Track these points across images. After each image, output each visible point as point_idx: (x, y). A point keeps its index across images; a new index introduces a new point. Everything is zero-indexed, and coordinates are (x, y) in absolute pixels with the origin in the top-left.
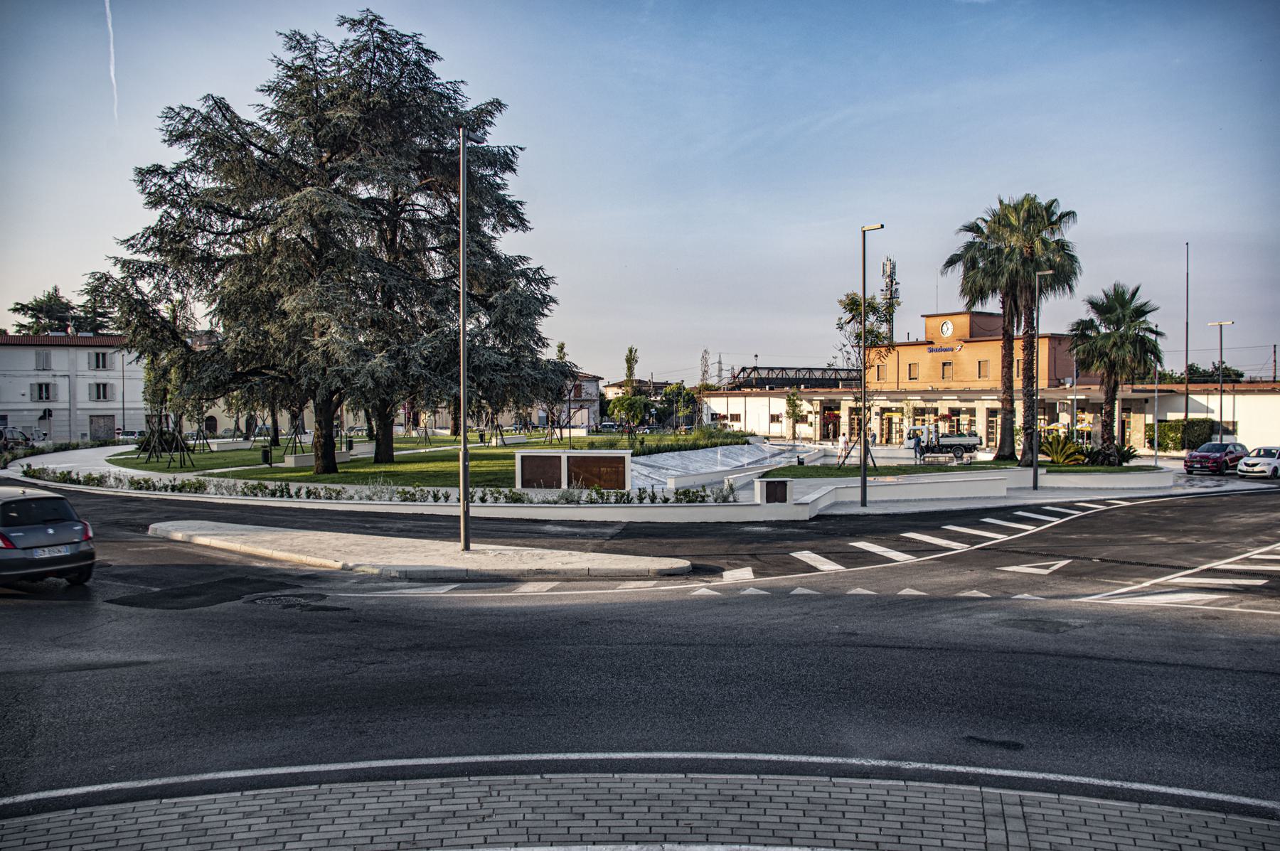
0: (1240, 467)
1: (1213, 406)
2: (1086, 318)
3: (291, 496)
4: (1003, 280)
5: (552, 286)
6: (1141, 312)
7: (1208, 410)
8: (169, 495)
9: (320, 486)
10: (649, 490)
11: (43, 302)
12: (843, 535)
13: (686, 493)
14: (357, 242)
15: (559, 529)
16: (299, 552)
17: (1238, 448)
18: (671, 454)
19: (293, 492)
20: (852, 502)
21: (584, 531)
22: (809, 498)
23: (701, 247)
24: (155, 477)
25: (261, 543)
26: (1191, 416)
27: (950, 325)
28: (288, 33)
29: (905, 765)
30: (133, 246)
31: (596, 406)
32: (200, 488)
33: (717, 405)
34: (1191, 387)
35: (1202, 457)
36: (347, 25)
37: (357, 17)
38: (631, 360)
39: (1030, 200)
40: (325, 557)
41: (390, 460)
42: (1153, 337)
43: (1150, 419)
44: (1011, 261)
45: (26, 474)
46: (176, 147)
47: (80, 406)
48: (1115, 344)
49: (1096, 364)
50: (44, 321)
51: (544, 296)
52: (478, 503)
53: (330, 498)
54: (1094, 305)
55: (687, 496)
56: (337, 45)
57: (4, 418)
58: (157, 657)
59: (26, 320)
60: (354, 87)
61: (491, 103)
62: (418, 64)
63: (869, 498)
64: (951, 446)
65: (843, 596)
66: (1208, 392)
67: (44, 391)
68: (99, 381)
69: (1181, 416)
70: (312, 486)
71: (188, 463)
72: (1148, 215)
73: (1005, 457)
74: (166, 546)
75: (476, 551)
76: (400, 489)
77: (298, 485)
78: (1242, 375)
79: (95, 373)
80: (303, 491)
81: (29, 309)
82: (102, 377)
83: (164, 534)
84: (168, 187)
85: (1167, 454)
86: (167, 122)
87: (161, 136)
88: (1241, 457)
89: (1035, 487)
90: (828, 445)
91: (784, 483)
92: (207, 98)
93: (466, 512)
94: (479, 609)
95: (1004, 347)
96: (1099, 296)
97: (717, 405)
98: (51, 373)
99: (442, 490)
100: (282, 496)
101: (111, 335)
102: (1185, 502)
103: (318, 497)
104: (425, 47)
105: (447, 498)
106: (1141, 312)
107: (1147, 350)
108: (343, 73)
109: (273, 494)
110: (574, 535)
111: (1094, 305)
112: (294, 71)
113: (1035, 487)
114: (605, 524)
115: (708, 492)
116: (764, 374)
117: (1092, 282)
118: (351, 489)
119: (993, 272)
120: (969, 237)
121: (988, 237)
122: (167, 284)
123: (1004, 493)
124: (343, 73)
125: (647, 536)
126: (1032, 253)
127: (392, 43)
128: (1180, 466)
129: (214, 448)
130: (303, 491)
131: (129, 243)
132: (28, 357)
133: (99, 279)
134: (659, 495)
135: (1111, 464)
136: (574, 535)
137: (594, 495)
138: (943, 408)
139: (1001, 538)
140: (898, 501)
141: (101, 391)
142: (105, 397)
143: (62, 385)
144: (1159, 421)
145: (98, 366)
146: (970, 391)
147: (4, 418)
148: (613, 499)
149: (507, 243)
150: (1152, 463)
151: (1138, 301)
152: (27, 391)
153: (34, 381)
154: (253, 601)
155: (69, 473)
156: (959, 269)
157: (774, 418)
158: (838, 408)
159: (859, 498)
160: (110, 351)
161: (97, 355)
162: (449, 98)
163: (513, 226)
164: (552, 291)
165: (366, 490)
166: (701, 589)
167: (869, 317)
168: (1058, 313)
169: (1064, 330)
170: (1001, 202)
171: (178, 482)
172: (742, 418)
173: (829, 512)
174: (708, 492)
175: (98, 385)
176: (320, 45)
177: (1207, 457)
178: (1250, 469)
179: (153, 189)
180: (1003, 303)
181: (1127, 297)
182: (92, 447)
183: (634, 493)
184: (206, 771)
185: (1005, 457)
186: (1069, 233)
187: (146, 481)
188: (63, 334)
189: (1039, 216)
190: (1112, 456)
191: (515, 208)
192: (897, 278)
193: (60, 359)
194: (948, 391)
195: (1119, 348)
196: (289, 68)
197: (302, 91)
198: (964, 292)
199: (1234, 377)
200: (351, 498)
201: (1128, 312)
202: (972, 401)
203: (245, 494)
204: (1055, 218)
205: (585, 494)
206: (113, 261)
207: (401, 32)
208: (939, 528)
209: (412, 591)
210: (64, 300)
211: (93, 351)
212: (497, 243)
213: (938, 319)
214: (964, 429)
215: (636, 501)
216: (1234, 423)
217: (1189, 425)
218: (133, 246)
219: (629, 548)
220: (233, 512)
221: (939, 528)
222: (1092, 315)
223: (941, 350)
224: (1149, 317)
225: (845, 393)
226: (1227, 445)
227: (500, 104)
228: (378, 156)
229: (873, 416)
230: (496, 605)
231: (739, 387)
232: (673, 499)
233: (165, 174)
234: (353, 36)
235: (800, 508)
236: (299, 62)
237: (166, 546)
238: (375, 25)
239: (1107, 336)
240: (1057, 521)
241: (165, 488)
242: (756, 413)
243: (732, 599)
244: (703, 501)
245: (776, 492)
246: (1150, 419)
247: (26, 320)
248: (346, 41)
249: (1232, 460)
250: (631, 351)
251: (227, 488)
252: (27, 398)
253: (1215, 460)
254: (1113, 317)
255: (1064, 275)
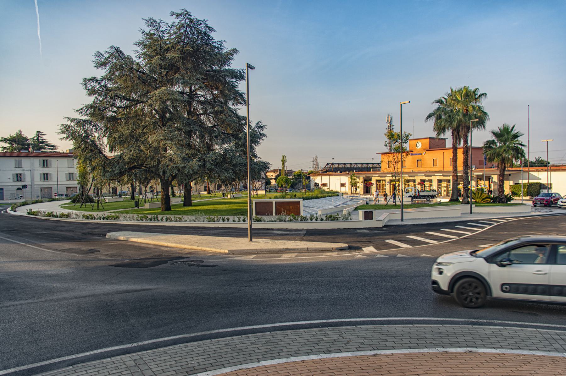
0: (559, 203)
1: (542, 177)
2: (491, 139)
3: (158, 221)
4: (455, 124)
5: (264, 129)
6: (516, 136)
7: (538, 179)
8: (102, 221)
9: (172, 216)
10: (315, 216)
11: (14, 137)
12: (401, 233)
13: (330, 216)
14: (174, 110)
15: (280, 232)
16: (180, 243)
17: (557, 195)
18: (308, 201)
19: (159, 219)
20: (396, 220)
21: (291, 233)
22: (381, 218)
23: (322, 112)
24: (94, 214)
25: (161, 240)
26: (531, 181)
27: (420, 144)
28: (147, 19)
29: (494, 321)
30: (82, 113)
31: (264, 181)
32: (117, 218)
33: (319, 180)
34: (531, 169)
35: (541, 199)
36: (174, 16)
37: (179, 12)
38: (284, 161)
39: (466, 88)
40: (192, 245)
41: (190, 204)
42: (520, 147)
43: (511, 183)
44: (458, 115)
45: (29, 213)
46: (100, 69)
47: (35, 183)
48: (505, 150)
49: (496, 159)
50: (15, 146)
51: (261, 134)
52: (242, 222)
53: (176, 221)
54: (495, 134)
55: (331, 218)
56: (170, 25)
57: (2, 189)
58: (156, 287)
59: (7, 145)
60: (178, 43)
61: (232, 50)
62: (205, 33)
63: (404, 218)
64: (425, 196)
65: (419, 258)
66: (538, 171)
67: (18, 177)
68: (44, 172)
69: (526, 181)
70: (168, 216)
71: (101, 207)
72: (515, 97)
73: (454, 200)
74: (119, 243)
75: (256, 242)
76: (208, 217)
77: (162, 216)
78: (549, 163)
79: (42, 169)
80: (164, 219)
81: (8, 140)
82: (46, 170)
83: (115, 237)
84: (98, 87)
85: (521, 198)
86: (97, 58)
87: (93, 64)
88: (558, 199)
89: (471, 213)
90: (369, 196)
91: (372, 212)
92: (111, 47)
93: (251, 226)
94: (273, 265)
95: (453, 153)
96: (497, 130)
97: (319, 180)
98: (22, 169)
99: (226, 217)
100: (155, 221)
101: (46, 152)
102: (540, 218)
103: (171, 221)
104: (209, 26)
105: (228, 220)
106: (516, 136)
107: (518, 153)
108: (172, 37)
109: (151, 220)
110: (288, 235)
111: (495, 134)
112: (150, 36)
113: (471, 213)
114: (297, 230)
115: (340, 216)
116: (336, 166)
117: (494, 124)
118: (186, 217)
119: (450, 120)
120: (437, 105)
121: (446, 105)
122: (92, 129)
123: (460, 216)
124: (172, 37)
125: (319, 234)
126: (467, 112)
127: (194, 24)
128: (531, 203)
129: (107, 201)
130: (164, 219)
131: (80, 111)
132: (11, 162)
133: (65, 127)
134: (319, 218)
135: (503, 202)
136: (288, 235)
137: (292, 218)
138: (418, 180)
139: (470, 234)
140: (415, 219)
141: (46, 177)
142: (47, 179)
143: (27, 175)
144: (516, 184)
145: (44, 166)
146: (430, 172)
147: (2, 189)
148: (299, 219)
149: (241, 110)
150: (521, 202)
151: (514, 132)
152: (11, 177)
153: (14, 172)
154: (173, 264)
155: (52, 212)
156: (433, 119)
157: (343, 185)
158: (371, 180)
159: (400, 218)
160: (49, 159)
161: (44, 161)
162: (218, 48)
163: (241, 103)
164: (264, 132)
165: (193, 218)
166: (357, 255)
167: (397, 142)
168: (479, 137)
169: (481, 145)
170: (452, 90)
171: (106, 216)
172: (328, 185)
173: (389, 224)
174: (340, 216)
175: (44, 174)
176: (162, 24)
177: (543, 199)
178: (564, 204)
179: (90, 88)
180: (453, 133)
181: (510, 129)
182: (48, 201)
183: (308, 216)
184: (213, 329)
185: (454, 200)
186: (484, 104)
187: (91, 215)
188: (27, 151)
189: (470, 96)
190: (502, 200)
191: (242, 96)
192: (393, 124)
193: (26, 163)
194: (419, 172)
195: (506, 152)
196: (147, 34)
197: (154, 44)
198: (435, 129)
199: (545, 164)
200: (186, 221)
201: (510, 136)
202: (431, 176)
203: (138, 220)
204: (477, 96)
205: (288, 218)
206: (67, 119)
207: (199, 19)
208: (440, 230)
209: (243, 258)
210: (24, 136)
211: (42, 159)
212: (238, 111)
213: (415, 141)
214: (427, 188)
215: (309, 220)
216: (551, 184)
217: (530, 185)
218: (82, 113)
219: (316, 239)
220: (135, 228)
221: (440, 230)
222: (494, 138)
223: (416, 154)
224: (519, 138)
225: (374, 174)
226: (552, 194)
227: (236, 50)
228: (189, 74)
229: (387, 183)
230: (274, 263)
231: (326, 172)
232: (325, 219)
233: (97, 81)
234: (177, 21)
235: (379, 222)
236: (152, 32)
237: (119, 243)
238: (187, 16)
239: (500, 147)
240: (489, 227)
241: (100, 218)
242: (334, 182)
243: (371, 259)
244: (338, 220)
245: (368, 216)
246: (511, 183)
247: (7, 145)
248: (174, 23)
249: (554, 200)
250: (283, 157)
251: (129, 218)
252: (11, 180)
253: (547, 200)
254: (503, 139)
255: (481, 122)
